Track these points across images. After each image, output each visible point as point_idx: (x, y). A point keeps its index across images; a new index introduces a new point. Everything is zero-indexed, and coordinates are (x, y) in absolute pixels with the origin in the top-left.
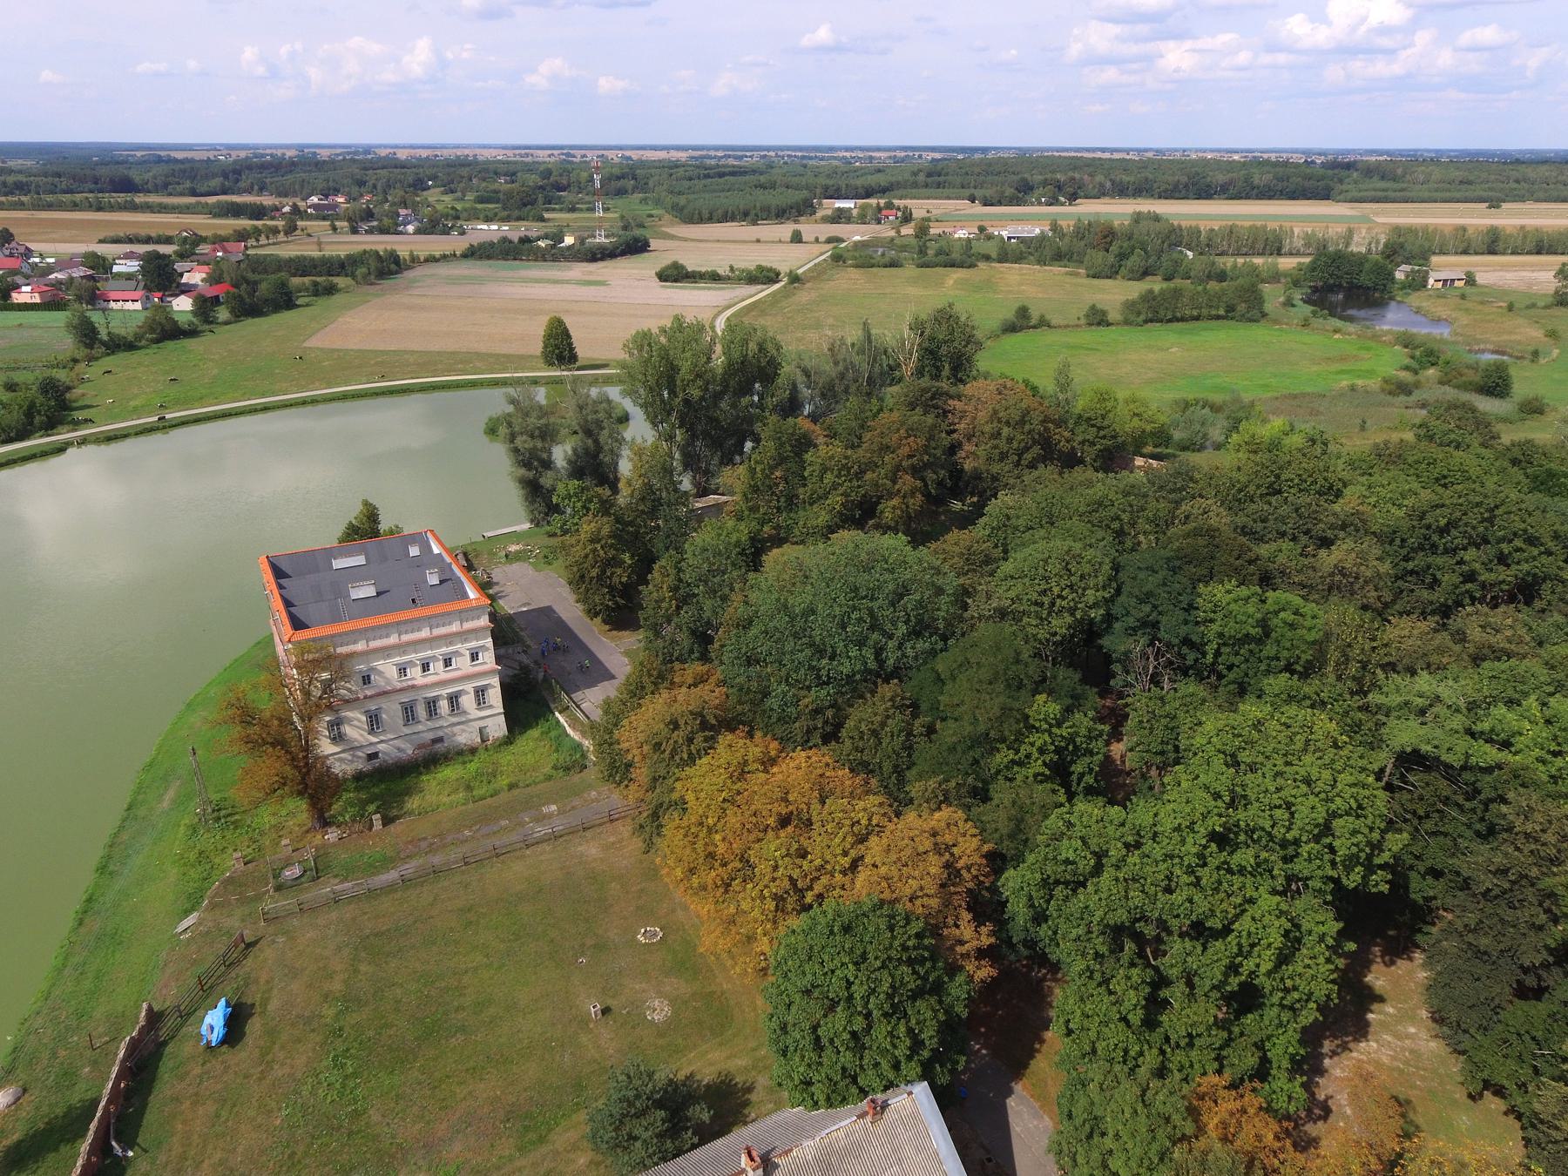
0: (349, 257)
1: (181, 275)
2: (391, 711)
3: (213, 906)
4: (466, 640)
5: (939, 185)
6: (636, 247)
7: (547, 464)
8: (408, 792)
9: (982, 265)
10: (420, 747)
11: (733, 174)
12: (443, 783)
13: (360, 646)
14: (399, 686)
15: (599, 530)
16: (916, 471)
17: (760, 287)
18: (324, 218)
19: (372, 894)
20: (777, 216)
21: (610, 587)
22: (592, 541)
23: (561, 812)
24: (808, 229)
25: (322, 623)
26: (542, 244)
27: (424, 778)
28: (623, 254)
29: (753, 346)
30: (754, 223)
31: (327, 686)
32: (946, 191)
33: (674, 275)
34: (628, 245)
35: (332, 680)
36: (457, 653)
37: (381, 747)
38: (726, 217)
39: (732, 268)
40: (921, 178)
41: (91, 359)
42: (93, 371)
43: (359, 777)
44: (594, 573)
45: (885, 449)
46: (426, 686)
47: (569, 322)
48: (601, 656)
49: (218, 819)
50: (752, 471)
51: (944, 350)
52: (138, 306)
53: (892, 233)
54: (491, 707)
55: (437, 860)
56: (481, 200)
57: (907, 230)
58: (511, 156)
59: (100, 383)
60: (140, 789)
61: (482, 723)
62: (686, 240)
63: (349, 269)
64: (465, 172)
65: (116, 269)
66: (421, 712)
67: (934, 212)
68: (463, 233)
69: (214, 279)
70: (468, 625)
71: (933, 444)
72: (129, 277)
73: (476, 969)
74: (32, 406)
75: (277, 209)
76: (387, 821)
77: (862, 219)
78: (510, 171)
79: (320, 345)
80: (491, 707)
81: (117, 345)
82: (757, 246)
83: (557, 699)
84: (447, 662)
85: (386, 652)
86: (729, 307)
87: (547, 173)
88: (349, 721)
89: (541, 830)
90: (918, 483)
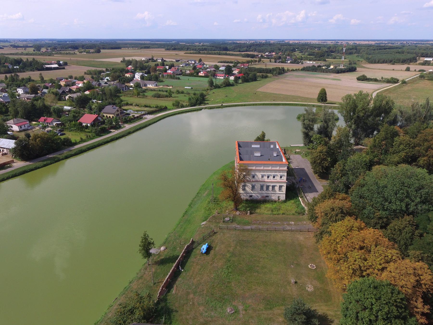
0: (272, 69)
2: (258, 186)
3: (209, 221)
4: (280, 172)
7: (312, 129)
8: (257, 208)
10: (263, 197)
11: (389, 48)
12: (266, 208)
13: (254, 168)
17: (391, 84)
18: (268, 58)
19: (244, 230)
20: (402, 62)
22: (320, 152)
23: (294, 225)
24: (412, 67)
26: (324, 68)
27: (262, 205)
28: (347, 72)
29: (384, 102)
31: (244, 176)
36: (277, 175)
38: (384, 62)
39: (382, 78)
41: (211, 89)
42: (211, 92)
43: (247, 200)
44: (319, 161)
46: (267, 182)
48: (315, 185)
54: (282, 191)
55: (261, 227)
56: (309, 55)
59: (214, 96)
61: (279, 195)
62: (368, 68)
65: (220, 69)
66: (265, 188)
68: (302, 64)
69: (240, 73)
70: (281, 169)
72: (222, 71)
73: (264, 258)
74: (198, 99)
75: (257, 56)
76: (251, 213)
78: (319, 47)
79: (260, 90)
80: (282, 191)
82: (393, 71)
84: (274, 177)
85: (260, 171)
88: (247, 186)
89: (288, 228)
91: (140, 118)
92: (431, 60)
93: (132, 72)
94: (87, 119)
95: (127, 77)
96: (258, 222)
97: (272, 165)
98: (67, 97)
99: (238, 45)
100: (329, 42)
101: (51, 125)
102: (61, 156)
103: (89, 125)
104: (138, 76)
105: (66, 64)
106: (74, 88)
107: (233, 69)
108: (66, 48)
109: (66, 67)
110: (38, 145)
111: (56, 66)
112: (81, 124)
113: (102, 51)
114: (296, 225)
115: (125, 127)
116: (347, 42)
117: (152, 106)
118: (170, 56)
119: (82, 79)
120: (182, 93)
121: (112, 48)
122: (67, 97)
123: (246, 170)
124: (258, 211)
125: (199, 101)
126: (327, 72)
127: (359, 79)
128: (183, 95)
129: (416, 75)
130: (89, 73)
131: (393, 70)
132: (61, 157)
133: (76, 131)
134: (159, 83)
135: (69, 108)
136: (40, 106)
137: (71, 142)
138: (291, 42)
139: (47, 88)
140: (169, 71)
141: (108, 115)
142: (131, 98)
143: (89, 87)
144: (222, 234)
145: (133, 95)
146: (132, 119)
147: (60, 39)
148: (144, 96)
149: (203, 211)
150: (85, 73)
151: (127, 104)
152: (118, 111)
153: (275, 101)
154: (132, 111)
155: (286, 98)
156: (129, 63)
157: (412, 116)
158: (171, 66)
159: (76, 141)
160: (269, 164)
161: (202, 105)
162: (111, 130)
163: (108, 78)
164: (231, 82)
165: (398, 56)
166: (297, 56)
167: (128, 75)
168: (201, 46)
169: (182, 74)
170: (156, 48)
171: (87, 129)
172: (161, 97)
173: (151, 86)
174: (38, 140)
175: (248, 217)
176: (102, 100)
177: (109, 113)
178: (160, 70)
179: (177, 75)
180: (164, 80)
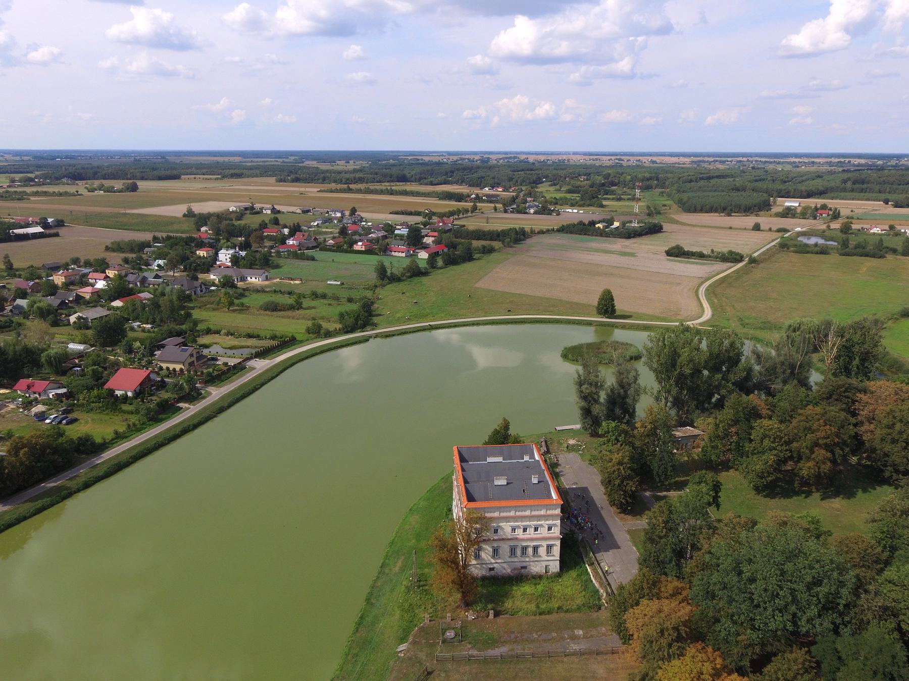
0: (503, 231)
1: (423, 237)
2: (505, 548)
5: (862, 191)
6: (654, 230)
7: (596, 401)
9: (890, 257)
10: (515, 569)
11: (718, 177)
12: (524, 594)
13: (496, 514)
14: (509, 537)
15: (623, 457)
16: (827, 447)
17: (729, 264)
18: (491, 202)
19: (486, 661)
20: (745, 211)
21: (625, 491)
23: (585, 637)
24: (764, 220)
25: (481, 500)
26: (600, 225)
27: (515, 588)
28: (647, 234)
29: (726, 342)
30: (729, 215)
32: (867, 195)
33: (676, 253)
34: (650, 228)
35: (480, 532)
36: (542, 526)
37: (495, 565)
38: (712, 210)
39: (712, 251)
40: (849, 185)
41: (383, 286)
42: (382, 293)
43: (484, 578)
45: (809, 430)
46: (523, 540)
47: (614, 294)
48: (614, 530)
49: (419, 587)
50: (717, 426)
51: (856, 349)
52: (404, 255)
53: (824, 227)
55: (518, 649)
56: (569, 192)
57: (835, 225)
58: (588, 161)
60: (386, 557)
61: (547, 563)
62: (684, 224)
63: (501, 238)
64: (562, 173)
65: (397, 232)
66: (519, 552)
67: (856, 211)
68: (558, 214)
69: (438, 242)
70: (549, 512)
71: (842, 431)
72: (401, 236)
74: (358, 316)
75: (469, 196)
76: (497, 614)
77: (804, 215)
78: (588, 171)
79: (483, 286)
81: (395, 279)
82: (729, 232)
83: (587, 555)
84: (536, 529)
85: (507, 519)
86: (707, 279)
87: (607, 176)
88: (484, 550)
89: (574, 647)
90: (829, 455)
91: (240, 368)
92: (797, 205)
93: (211, 246)
94: (125, 382)
95: (200, 257)
96: (513, 636)
97: (532, 508)
98: (73, 319)
99: (429, 168)
100: (604, 158)
101: (43, 397)
102: (75, 482)
103: (130, 394)
104: (225, 256)
105: (60, 223)
106: (86, 292)
107: (424, 232)
108: (57, 179)
109: (61, 231)
110: (22, 464)
111: (38, 229)
112: (111, 392)
113: (141, 184)
114: (587, 638)
115: (209, 394)
116: (638, 158)
117: (262, 334)
118: (289, 199)
119: (101, 266)
120: (324, 296)
121: (161, 178)
122: (73, 319)
123: (481, 519)
124: (508, 604)
125: (362, 319)
126: (608, 235)
127: (669, 253)
128: (325, 301)
129: (773, 241)
130: (117, 247)
131: (731, 228)
132: (73, 484)
133: (101, 410)
134: (272, 271)
135: (81, 347)
136: (15, 352)
137: (93, 444)
138: (531, 159)
139: (23, 295)
140: (291, 242)
141: (171, 366)
142: (215, 313)
143: (120, 290)
144: (443, 675)
145: (217, 306)
146: (224, 373)
147: (40, 151)
148: (244, 309)
149: (398, 613)
150: (107, 249)
151: (208, 331)
152: (192, 355)
153: (514, 311)
154: (222, 350)
155: (537, 304)
156: (203, 219)
157: (779, 366)
158: (295, 230)
159: (104, 439)
160: (526, 506)
161: (368, 328)
162: (181, 405)
163: (161, 262)
164: (423, 265)
165: (736, 198)
166: (548, 197)
167: (201, 253)
168: (351, 172)
169: (320, 246)
170: (256, 176)
171: (125, 403)
172: (280, 310)
173: (254, 280)
174: (22, 452)
175: (494, 625)
176: (153, 323)
177: (172, 361)
178: (270, 238)
179: (308, 248)
180: (281, 262)
